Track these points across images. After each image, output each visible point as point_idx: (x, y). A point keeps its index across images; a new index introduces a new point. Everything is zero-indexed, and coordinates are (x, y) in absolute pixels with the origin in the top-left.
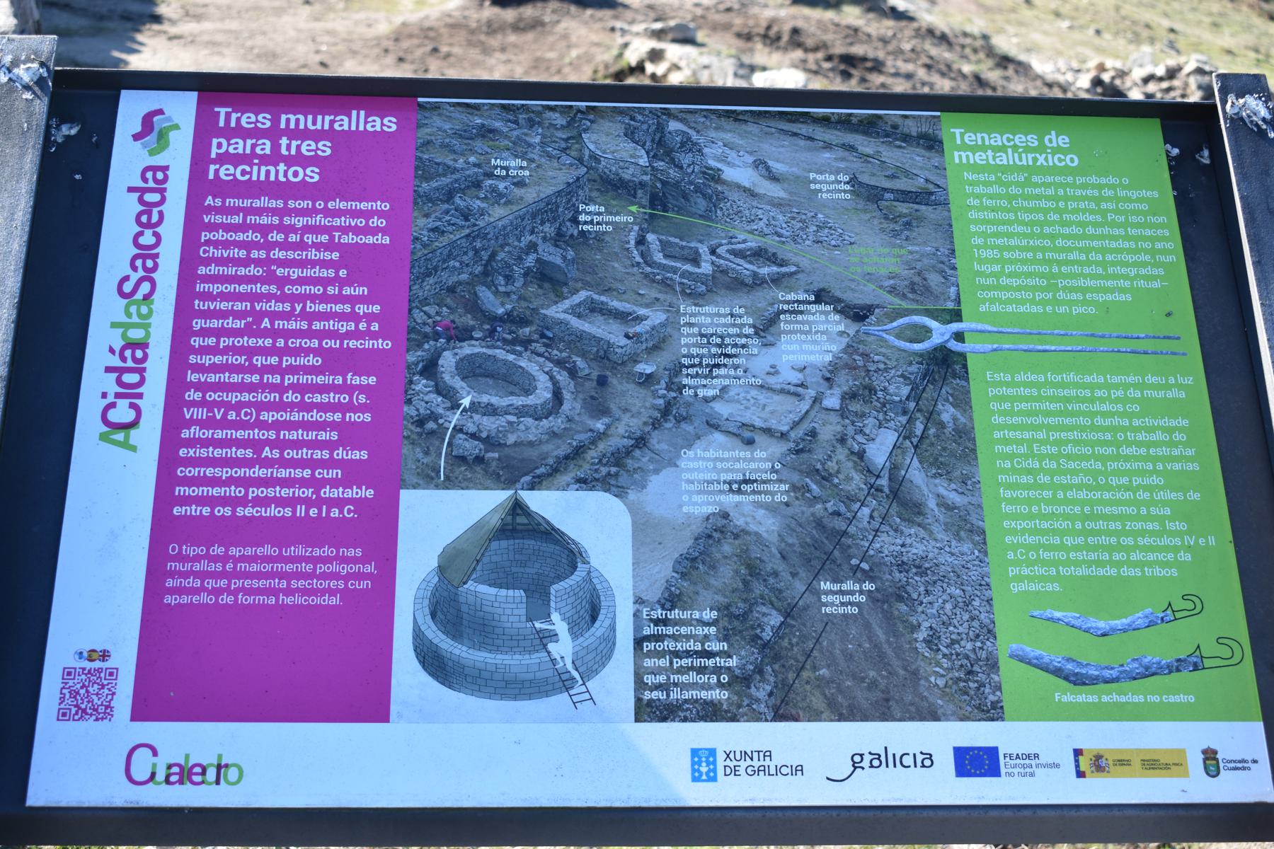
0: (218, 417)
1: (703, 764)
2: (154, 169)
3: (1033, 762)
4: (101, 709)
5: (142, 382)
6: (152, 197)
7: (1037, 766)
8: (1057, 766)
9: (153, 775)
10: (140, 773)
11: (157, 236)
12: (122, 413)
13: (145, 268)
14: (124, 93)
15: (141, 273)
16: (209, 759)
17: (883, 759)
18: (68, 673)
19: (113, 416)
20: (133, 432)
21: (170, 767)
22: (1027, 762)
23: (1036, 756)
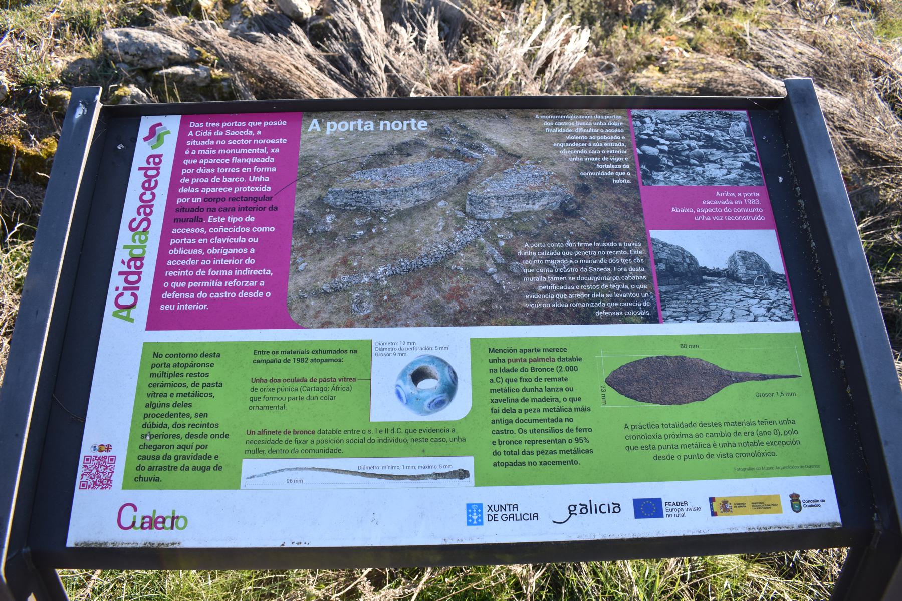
1: (474, 515)
2: (154, 156)
3: (684, 507)
4: (105, 482)
6: (152, 173)
7: (686, 509)
8: (699, 509)
9: (134, 523)
10: (126, 521)
11: (153, 195)
12: (127, 299)
13: (145, 213)
14: (143, 118)
15: (143, 216)
16: (167, 513)
17: (589, 508)
19: (122, 301)
20: (132, 310)
21: (144, 518)
22: (680, 507)
23: (686, 503)
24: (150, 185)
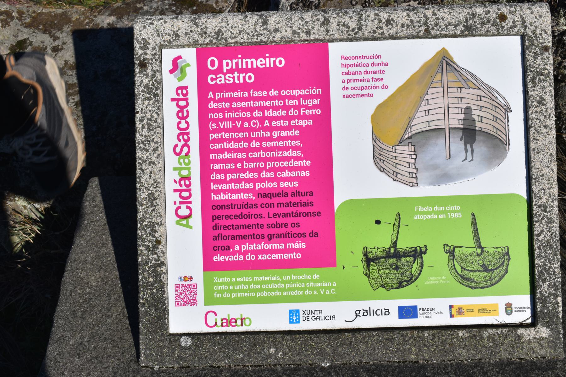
0: (239, 126)
1: (294, 315)
3: (432, 312)
4: (192, 301)
5: (190, 196)
6: (182, 103)
7: (433, 313)
8: (442, 313)
9: (216, 323)
10: (211, 322)
11: (187, 123)
12: (184, 211)
15: (183, 142)
16: (237, 316)
17: (368, 312)
18: (177, 287)
19: (180, 213)
20: (190, 220)
21: (222, 320)
22: (429, 311)
23: (434, 309)
24: (183, 114)
